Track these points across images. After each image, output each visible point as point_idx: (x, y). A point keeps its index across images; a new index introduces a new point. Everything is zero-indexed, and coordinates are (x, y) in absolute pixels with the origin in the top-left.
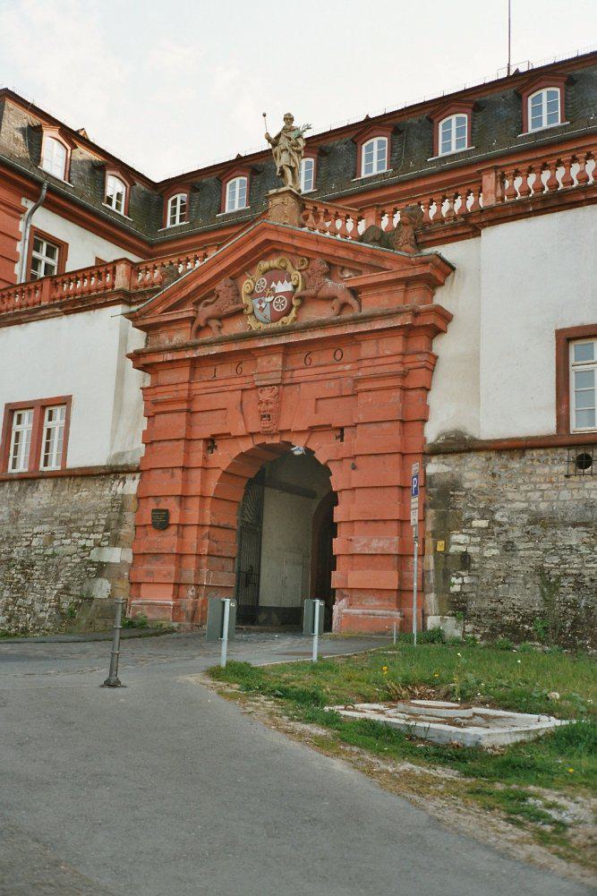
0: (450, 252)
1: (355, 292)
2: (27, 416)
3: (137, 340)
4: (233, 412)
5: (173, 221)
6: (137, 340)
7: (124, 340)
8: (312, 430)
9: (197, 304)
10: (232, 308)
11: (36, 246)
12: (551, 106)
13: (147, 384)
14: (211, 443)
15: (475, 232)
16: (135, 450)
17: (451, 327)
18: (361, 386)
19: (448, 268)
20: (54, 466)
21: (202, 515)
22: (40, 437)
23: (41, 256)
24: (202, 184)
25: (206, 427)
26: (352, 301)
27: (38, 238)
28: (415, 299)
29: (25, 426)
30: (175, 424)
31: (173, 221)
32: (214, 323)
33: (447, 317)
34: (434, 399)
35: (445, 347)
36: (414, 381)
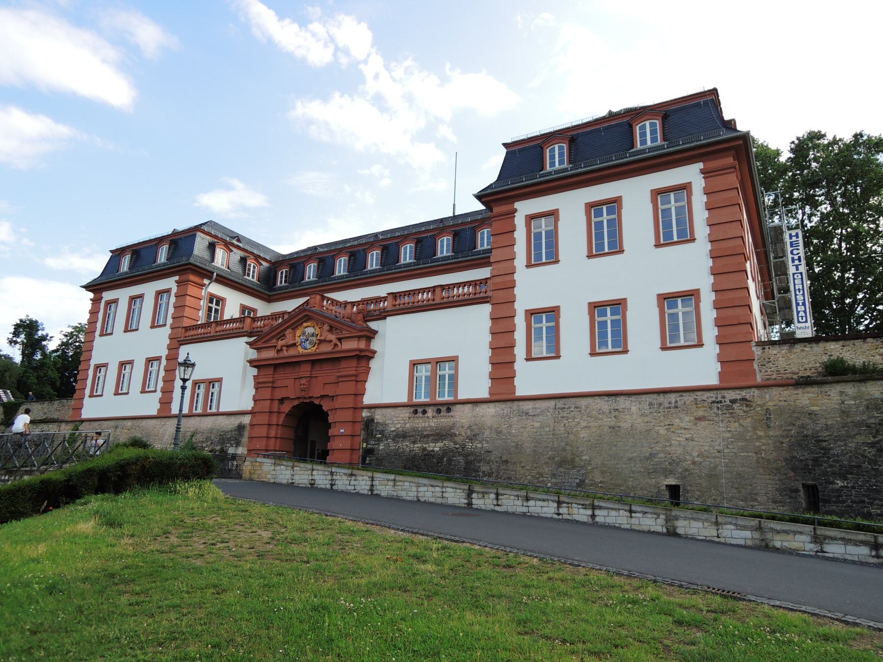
0: (373, 325)
1: (340, 339)
2: (202, 386)
3: (253, 354)
4: (291, 387)
5: (281, 282)
6: (253, 354)
7: (246, 354)
8: (322, 397)
9: (278, 339)
10: (292, 342)
11: (211, 301)
12: (561, 155)
13: (256, 374)
14: (282, 401)
15: (384, 318)
16: (249, 405)
17: (376, 355)
18: (341, 379)
19: (375, 332)
20: (214, 410)
21: (276, 433)
22: (431, 380)
23: (214, 306)
24: (295, 263)
25: (280, 394)
26: (339, 343)
27: (211, 298)
28: (362, 345)
29: (202, 391)
30: (267, 393)
31: (281, 282)
32: (284, 348)
33: (374, 352)
34: (368, 385)
35: (373, 364)
36: (360, 380)
